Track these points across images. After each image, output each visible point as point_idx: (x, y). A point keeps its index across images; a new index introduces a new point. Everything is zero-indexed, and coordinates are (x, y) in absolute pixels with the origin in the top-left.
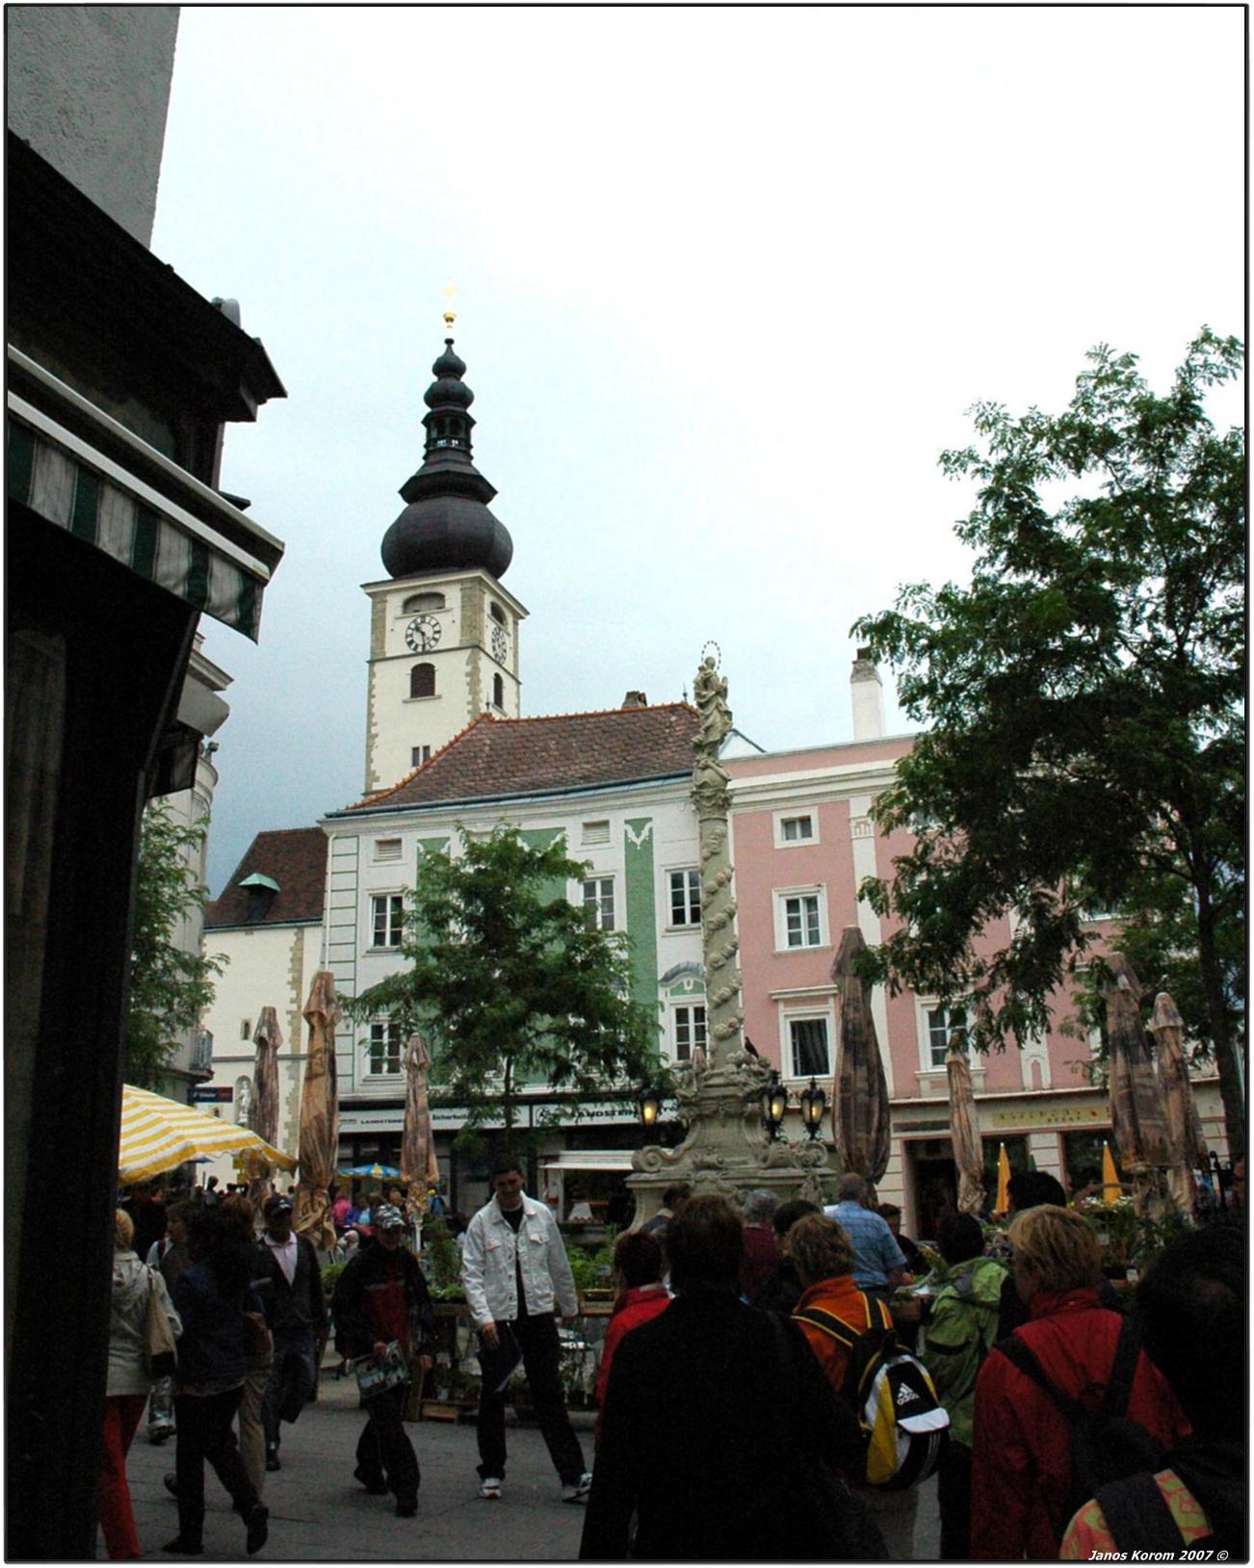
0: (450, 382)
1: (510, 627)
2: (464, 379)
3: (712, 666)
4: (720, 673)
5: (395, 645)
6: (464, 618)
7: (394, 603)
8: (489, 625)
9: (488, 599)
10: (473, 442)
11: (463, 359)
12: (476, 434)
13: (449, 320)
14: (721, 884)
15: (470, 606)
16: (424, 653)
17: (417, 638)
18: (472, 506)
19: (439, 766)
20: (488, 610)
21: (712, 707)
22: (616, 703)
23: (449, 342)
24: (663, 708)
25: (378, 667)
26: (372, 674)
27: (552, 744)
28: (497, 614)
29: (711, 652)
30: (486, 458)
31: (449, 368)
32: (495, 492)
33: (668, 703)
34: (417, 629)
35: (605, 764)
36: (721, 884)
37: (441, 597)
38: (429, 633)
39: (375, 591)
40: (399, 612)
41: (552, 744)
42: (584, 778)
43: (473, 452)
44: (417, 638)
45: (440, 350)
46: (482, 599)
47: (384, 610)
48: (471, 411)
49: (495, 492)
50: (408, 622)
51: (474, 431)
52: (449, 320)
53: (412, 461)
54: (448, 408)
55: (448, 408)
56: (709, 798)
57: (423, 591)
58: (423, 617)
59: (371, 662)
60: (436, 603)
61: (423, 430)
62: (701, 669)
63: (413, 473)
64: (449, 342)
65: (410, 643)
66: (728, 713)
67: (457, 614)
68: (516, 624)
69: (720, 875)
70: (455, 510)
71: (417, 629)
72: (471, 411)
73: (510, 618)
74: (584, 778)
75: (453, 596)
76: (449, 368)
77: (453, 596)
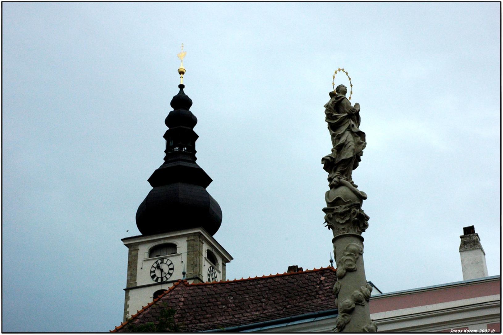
0: (182, 111)
1: (220, 267)
2: (191, 109)
3: (345, 92)
4: (353, 98)
5: (144, 278)
6: (189, 260)
7: (143, 251)
8: (206, 266)
9: (205, 247)
10: (197, 148)
11: (190, 97)
12: (199, 145)
13: (181, 73)
14: (358, 302)
15: (194, 253)
16: (163, 283)
17: (158, 273)
18: (196, 189)
19: (144, 317)
20: (205, 254)
21: (344, 128)
22: (283, 270)
23: (181, 87)
24: (315, 271)
25: (132, 293)
26: (127, 298)
27: (231, 299)
28: (211, 258)
29: (342, 80)
30: (205, 158)
31: (181, 102)
32: (212, 180)
33: (318, 268)
34: (158, 267)
35: (270, 310)
36: (358, 302)
37: (174, 246)
38: (166, 270)
39: (131, 244)
40: (146, 256)
41: (231, 299)
42: (254, 321)
43: (197, 155)
44: (158, 273)
45: (177, 91)
46: (201, 247)
47: (136, 255)
48: (196, 129)
49: (212, 180)
50: (152, 263)
51: (198, 143)
52: (181, 73)
53: (157, 160)
54: (181, 123)
55: (181, 123)
56: (343, 215)
57: (162, 242)
58: (162, 259)
59: (127, 290)
60: (171, 251)
61: (164, 141)
62: (332, 95)
63: (157, 167)
64: (181, 87)
65: (153, 277)
66: (362, 135)
67: (184, 258)
68: (224, 265)
69: (357, 292)
70: (184, 190)
71: (158, 267)
72: (196, 129)
73: (220, 261)
74: (254, 321)
75: (182, 245)
76: (181, 102)
77: (182, 245)
